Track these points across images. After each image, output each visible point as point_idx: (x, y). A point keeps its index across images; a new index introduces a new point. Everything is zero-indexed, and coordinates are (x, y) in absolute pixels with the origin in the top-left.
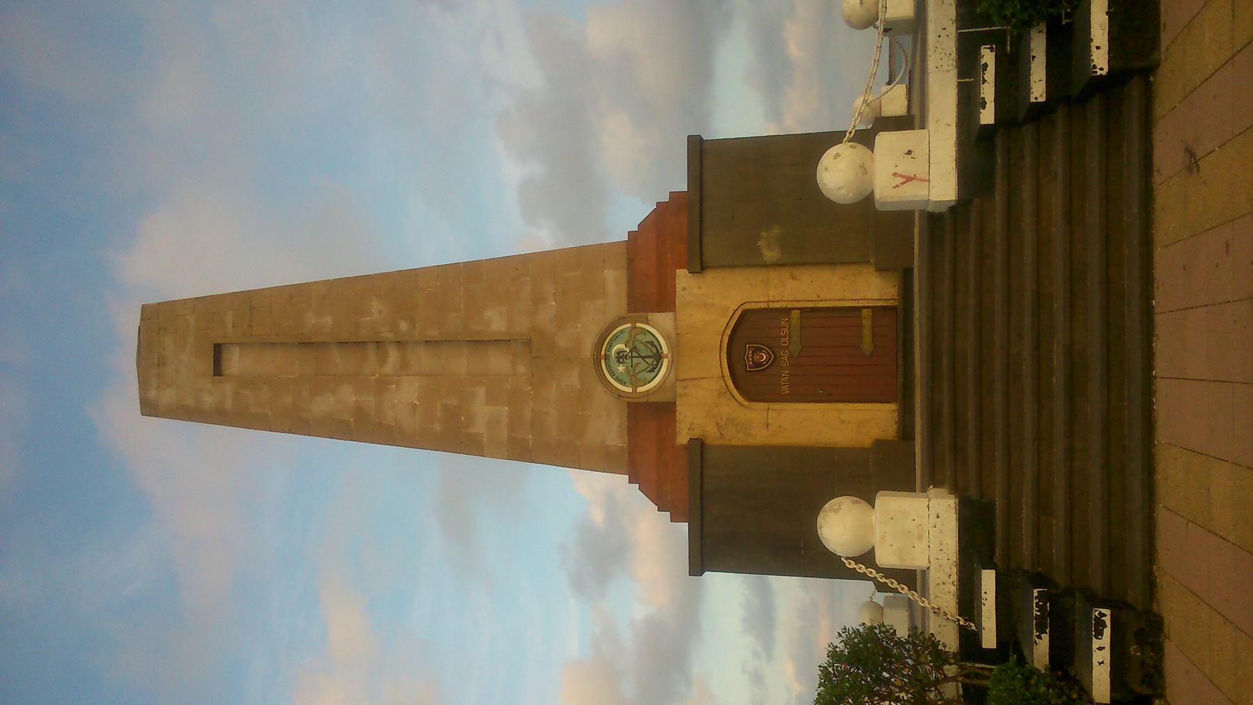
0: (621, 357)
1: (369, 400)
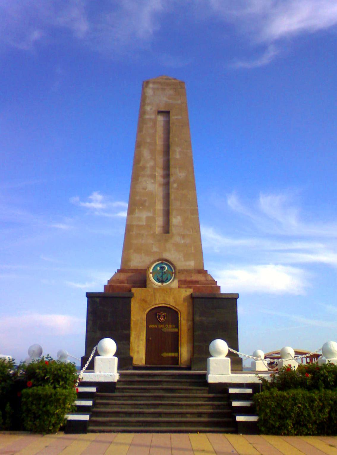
0: (162, 268)
1: (148, 172)
